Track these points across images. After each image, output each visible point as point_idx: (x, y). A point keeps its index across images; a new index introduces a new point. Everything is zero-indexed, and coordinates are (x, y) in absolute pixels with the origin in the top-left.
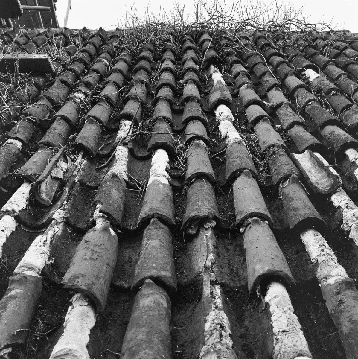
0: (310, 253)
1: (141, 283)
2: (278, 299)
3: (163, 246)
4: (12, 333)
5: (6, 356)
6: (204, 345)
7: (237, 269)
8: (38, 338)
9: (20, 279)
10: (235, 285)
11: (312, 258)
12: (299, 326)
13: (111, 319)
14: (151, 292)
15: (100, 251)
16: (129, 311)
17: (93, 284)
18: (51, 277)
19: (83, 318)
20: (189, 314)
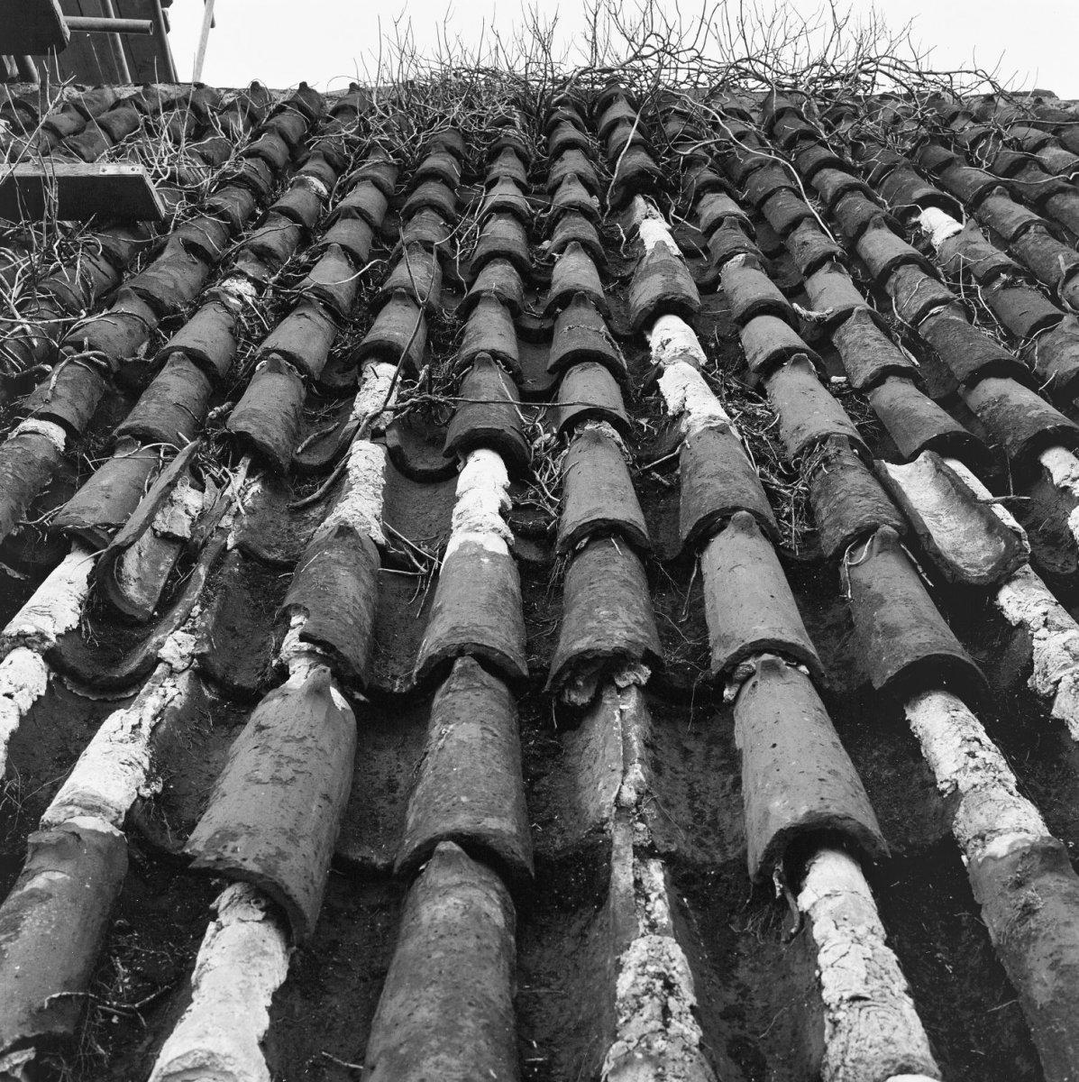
1: (426, 852)
2: (836, 902)
3: (492, 742)
4: (37, 1005)
5: (18, 1073)
6: (616, 1040)
7: (715, 812)
8: (115, 1020)
9: (61, 842)
10: (707, 858)
11: (939, 778)
12: (900, 983)
13: (335, 963)
14: (456, 879)
15: (300, 756)
16: (388, 937)
17: (281, 854)
18: (154, 836)
19: (249, 959)
20: (568, 945)
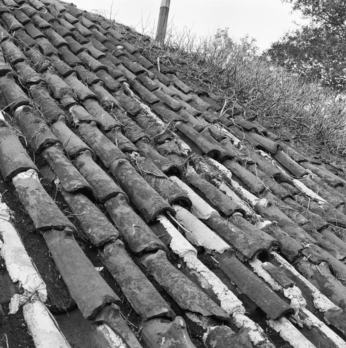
0: (26, 164)
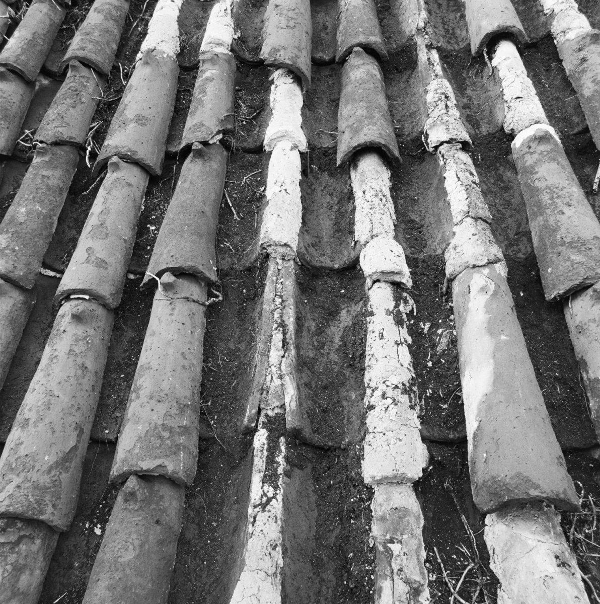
1: (349, 52)
2: (508, 62)
3: (366, 5)
4: (221, 119)
5: (218, 143)
6: (429, 118)
7: (453, 29)
8: (244, 123)
9: (212, 58)
10: (452, 48)
11: (545, 8)
12: (534, 91)
13: (317, 98)
14: (362, 62)
15: (295, 16)
16: (338, 87)
17: (297, 56)
18: (241, 54)
19: (291, 97)
20: (402, 86)
